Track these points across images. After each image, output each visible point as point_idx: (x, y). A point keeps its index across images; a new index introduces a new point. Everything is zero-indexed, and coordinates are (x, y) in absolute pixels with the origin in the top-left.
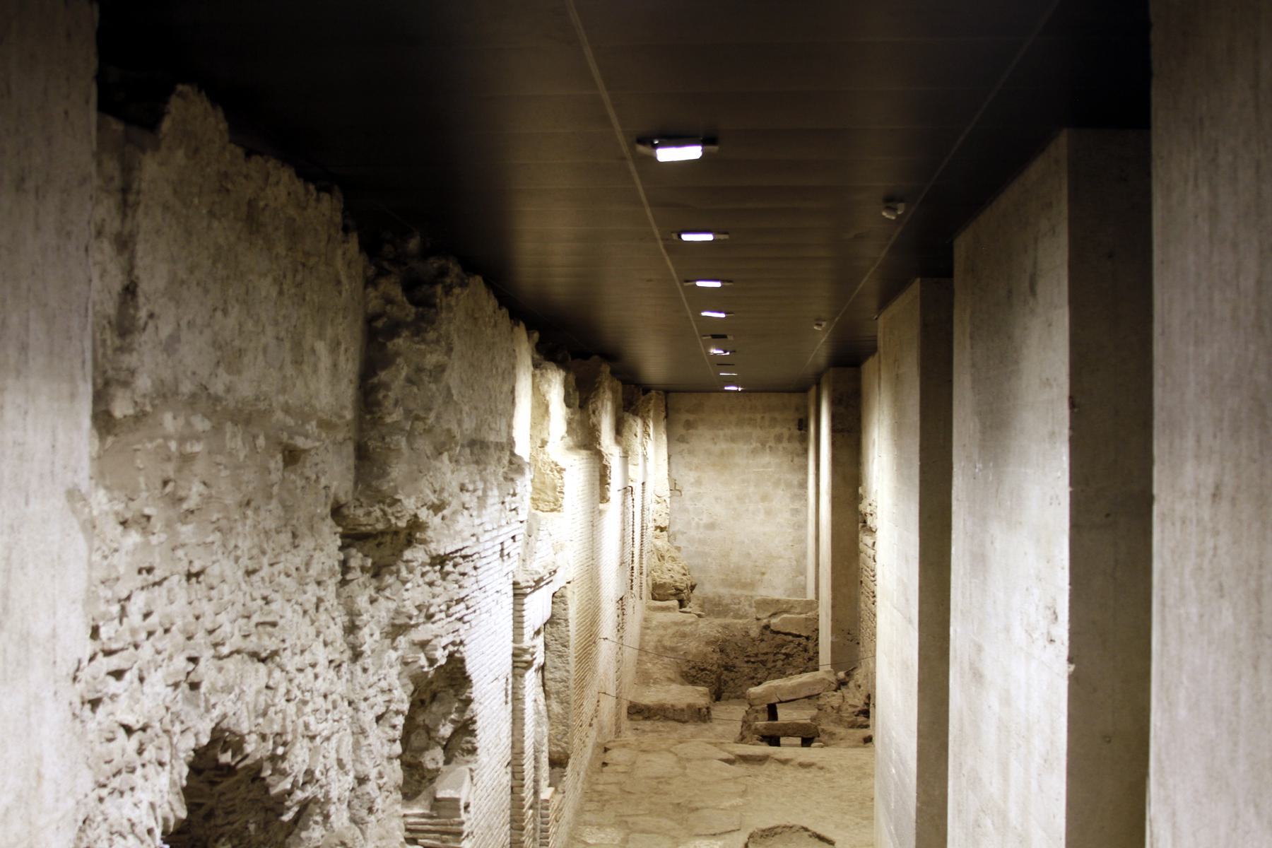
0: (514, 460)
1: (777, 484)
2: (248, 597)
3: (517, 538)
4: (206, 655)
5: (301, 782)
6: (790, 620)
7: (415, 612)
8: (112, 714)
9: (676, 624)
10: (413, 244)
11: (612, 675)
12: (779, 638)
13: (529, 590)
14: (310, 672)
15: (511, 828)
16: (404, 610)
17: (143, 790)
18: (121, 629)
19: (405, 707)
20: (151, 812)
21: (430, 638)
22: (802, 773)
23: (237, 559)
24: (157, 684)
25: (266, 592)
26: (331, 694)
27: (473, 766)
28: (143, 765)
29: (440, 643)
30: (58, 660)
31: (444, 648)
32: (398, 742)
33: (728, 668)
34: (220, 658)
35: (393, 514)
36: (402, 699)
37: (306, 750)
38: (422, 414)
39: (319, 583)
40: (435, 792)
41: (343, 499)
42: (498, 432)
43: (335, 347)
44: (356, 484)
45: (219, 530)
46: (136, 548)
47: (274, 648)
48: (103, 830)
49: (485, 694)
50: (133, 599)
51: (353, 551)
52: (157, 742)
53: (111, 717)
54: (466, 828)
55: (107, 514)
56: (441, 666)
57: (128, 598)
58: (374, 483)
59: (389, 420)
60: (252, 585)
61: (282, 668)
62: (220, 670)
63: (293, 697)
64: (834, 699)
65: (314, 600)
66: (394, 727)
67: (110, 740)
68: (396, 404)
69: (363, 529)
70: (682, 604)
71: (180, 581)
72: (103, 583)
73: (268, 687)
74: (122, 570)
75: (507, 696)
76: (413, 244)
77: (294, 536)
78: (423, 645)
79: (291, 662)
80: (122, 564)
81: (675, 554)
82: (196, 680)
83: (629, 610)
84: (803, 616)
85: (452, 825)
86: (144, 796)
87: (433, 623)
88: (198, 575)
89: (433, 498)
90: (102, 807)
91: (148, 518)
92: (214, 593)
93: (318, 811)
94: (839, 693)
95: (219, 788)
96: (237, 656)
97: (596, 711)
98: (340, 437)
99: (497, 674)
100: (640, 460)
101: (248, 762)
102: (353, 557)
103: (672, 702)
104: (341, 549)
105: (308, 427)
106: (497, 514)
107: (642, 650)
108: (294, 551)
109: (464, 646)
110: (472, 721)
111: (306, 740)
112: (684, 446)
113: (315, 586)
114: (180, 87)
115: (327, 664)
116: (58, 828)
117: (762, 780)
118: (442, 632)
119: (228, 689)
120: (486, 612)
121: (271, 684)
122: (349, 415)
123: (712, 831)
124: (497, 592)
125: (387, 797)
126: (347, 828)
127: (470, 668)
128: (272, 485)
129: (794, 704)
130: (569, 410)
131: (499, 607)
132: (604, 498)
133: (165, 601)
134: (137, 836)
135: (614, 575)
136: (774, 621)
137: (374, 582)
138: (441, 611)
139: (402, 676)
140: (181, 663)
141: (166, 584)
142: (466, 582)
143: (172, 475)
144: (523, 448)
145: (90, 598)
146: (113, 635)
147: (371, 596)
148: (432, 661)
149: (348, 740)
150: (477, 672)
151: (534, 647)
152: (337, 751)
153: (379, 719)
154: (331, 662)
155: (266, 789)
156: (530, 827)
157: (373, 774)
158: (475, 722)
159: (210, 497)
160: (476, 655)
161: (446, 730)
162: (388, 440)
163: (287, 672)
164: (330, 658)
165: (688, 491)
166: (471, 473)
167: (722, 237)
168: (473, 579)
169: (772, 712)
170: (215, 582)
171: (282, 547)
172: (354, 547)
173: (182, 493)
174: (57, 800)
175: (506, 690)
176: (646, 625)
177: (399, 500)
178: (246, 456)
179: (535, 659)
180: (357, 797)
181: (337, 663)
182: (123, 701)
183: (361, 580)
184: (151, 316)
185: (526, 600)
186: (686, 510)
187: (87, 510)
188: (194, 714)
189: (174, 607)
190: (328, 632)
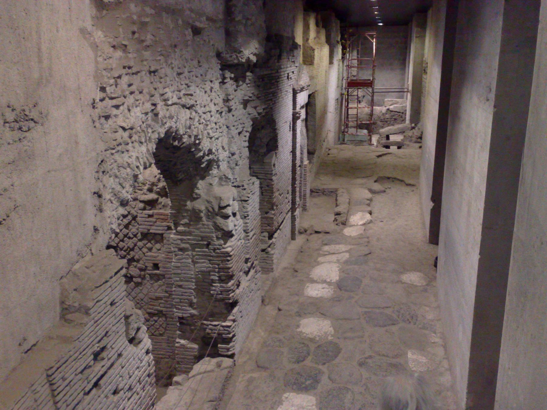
2: (179, 84)
3: (295, 72)
5: (207, 153)
12: (392, 113)
13: (298, 91)
18: (116, 89)
19: (250, 129)
20: (137, 160)
24: (137, 112)
25: (187, 82)
28: (132, 142)
30: (82, 98)
32: (247, 142)
34: (168, 106)
35: (240, 57)
37: (208, 142)
38: (250, 17)
39: (211, 81)
41: (221, 50)
44: (226, 45)
46: (120, 59)
53: (115, 123)
55: (104, 42)
58: (233, 44)
60: (180, 79)
62: (168, 110)
63: (201, 122)
64: (410, 133)
66: (245, 136)
67: (116, 132)
71: (146, 74)
72: (105, 70)
73: (190, 118)
75: (290, 128)
77: (199, 62)
80: (113, 63)
82: (157, 113)
86: (134, 155)
88: (154, 72)
91: (126, 46)
92: (162, 80)
93: (215, 164)
94: (412, 131)
95: (176, 155)
98: (218, 25)
101: (184, 145)
104: (220, 69)
105: (202, 19)
108: (199, 68)
109: (220, 83)
111: (209, 139)
113: (210, 83)
115: (216, 112)
116: (88, 163)
119: (171, 117)
121: (191, 117)
122: (221, 17)
128: (187, 41)
134: (131, 168)
135: (334, 90)
140: (148, 106)
141: (139, 74)
143: (136, 30)
144: (299, 40)
145: (97, 76)
146: (113, 91)
147: (234, 89)
152: (222, 143)
153: (240, 133)
154: (217, 111)
155: (194, 155)
157: (237, 152)
159: (156, 41)
162: (237, 27)
163: (199, 113)
164: (217, 109)
169: (388, 137)
170: (163, 76)
172: (227, 70)
173: (143, 38)
174: (87, 153)
175: (290, 126)
177: (242, 51)
178: (173, 27)
180: (231, 160)
181: (220, 111)
182: (121, 118)
187: (92, 38)
188: (156, 125)
189: (144, 84)
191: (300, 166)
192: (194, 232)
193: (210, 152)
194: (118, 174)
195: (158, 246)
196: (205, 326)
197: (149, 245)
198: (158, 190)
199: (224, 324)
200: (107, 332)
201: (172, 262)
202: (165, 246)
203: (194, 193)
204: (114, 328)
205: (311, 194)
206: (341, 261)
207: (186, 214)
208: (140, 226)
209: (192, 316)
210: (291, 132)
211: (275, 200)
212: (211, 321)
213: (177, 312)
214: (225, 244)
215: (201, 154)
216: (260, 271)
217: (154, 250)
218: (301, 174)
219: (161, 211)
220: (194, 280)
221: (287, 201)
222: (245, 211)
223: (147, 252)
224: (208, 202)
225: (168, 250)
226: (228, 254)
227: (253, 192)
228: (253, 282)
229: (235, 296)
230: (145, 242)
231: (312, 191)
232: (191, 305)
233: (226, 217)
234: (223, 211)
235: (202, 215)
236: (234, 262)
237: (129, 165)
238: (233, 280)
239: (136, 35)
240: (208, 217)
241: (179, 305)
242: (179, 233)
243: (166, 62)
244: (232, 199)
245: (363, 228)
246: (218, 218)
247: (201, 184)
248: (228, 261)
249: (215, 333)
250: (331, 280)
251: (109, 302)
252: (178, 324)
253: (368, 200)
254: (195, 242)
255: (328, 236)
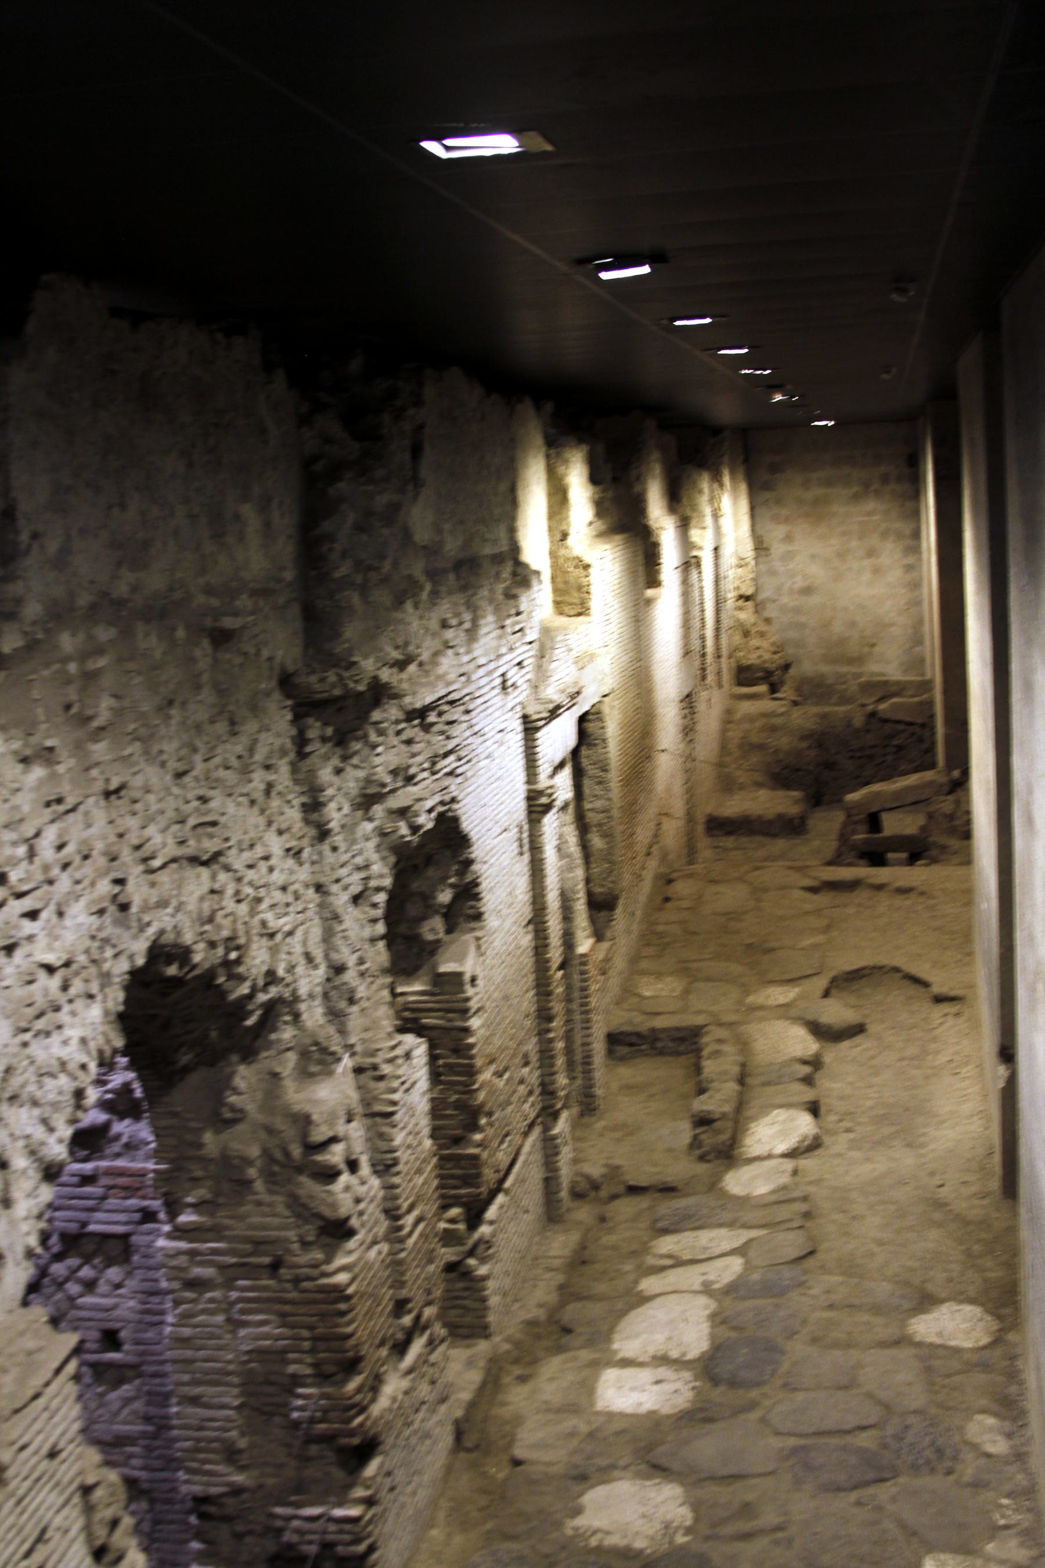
0: (519, 570)
1: (885, 535)
4: (135, 873)
6: (901, 704)
7: (388, 779)
8: (29, 955)
9: (765, 715)
10: (355, 365)
11: (678, 788)
12: (888, 728)
14: (263, 866)
15: (537, 994)
16: (375, 778)
17: (72, 1026)
18: (32, 867)
19: (388, 882)
21: (410, 803)
22: (899, 901)
23: (163, 764)
24: (79, 915)
26: (292, 884)
27: (479, 934)
29: (422, 806)
31: (430, 811)
33: (829, 766)
34: (152, 871)
36: (382, 874)
40: (435, 966)
41: (291, 668)
42: (495, 542)
43: (264, 505)
45: (138, 739)
46: (41, 782)
47: (216, 849)
48: (30, 1075)
49: (492, 849)
50: (44, 834)
51: (310, 721)
52: (84, 974)
54: (473, 1004)
56: (429, 831)
57: (37, 835)
59: (337, 574)
61: (227, 868)
65: (262, 787)
68: (344, 555)
69: (319, 696)
70: (774, 689)
71: (97, 802)
74: (26, 808)
75: (521, 846)
76: (355, 365)
77: (233, 723)
78: (403, 812)
79: (237, 860)
80: (25, 802)
81: (763, 627)
83: (701, 707)
84: (916, 699)
85: (458, 1002)
86: (74, 1033)
87: (415, 784)
88: (117, 791)
89: (396, 655)
90: (27, 1051)
91: (51, 749)
92: (138, 806)
94: (951, 798)
96: (174, 866)
97: (656, 836)
98: (281, 600)
99: (507, 824)
100: (709, 520)
101: (197, 972)
102: (310, 727)
103: (759, 812)
106: (494, 643)
107: (724, 748)
108: (233, 739)
109: (458, 802)
110: (475, 884)
112: (767, 495)
114: (45, 278)
117: (850, 910)
118: (425, 794)
119: (162, 904)
120: (487, 757)
122: (289, 575)
123: (787, 977)
124: (501, 731)
125: (372, 983)
126: (321, 1026)
127: (467, 825)
128: (199, 675)
129: (902, 809)
130: (597, 489)
131: (503, 748)
132: (653, 580)
133: (81, 826)
136: (882, 706)
137: (339, 751)
138: (424, 770)
139: (382, 847)
140: (105, 887)
141: (82, 808)
142: (455, 731)
143: (74, 697)
148: (415, 829)
149: (316, 932)
150: (477, 829)
151: (551, 787)
153: (356, 899)
154: (288, 850)
156: (560, 990)
157: (351, 960)
158: (477, 885)
160: (475, 809)
161: (445, 897)
163: (236, 871)
164: (288, 846)
165: (778, 549)
166: (456, 604)
167: (717, 319)
168: (465, 725)
169: (874, 822)
170: (137, 794)
171: (218, 738)
173: (89, 712)
175: (520, 840)
176: (728, 718)
177: (355, 663)
179: (554, 800)
180: (335, 988)
182: (42, 941)
183: (323, 751)
184: (35, 536)
185: (539, 735)
186: (773, 573)
188: (126, 935)
190: (282, 818)
191: (562, 966)
192: (228, 1228)
193: (271, 978)
194: (39, 1094)
195: (114, 1273)
196: (279, 1523)
197: (86, 1272)
198: (109, 1096)
199: (339, 1512)
200: (44, 1531)
201: (162, 1323)
202: (139, 1274)
203: (226, 1104)
204: (58, 1520)
205: (610, 1053)
206: (717, 1286)
207: (199, 1173)
208: (57, 1214)
209: (237, 1491)
210: (527, 857)
211: (481, 1096)
212: (299, 1505)
213: (186, 1482)
214: (328, 1260)
215: (245, 989)
216: (442, 1341)
217: (103, 1287)
218: (569, 988)
219: (121, 1163)
220: (236, 1380)
221: (522, 1089)
222: (385, 1148)
223: (81, 1296)
224: (270, 1131)
225: (148, 1285)
226: (338, 1293)
227: (406, 1086)
228: (423, 1376)
229: (369, 1423)
230: (73, 1262)
231: (613, 1039)
232: (231, 1455)
233: (330, 1175)
234: (319, 1158)
235: (252, 1172)
236: (360, 1318)
237: (63, 1064)
238: (360, 1373)
239: (74, 710)
240: (270, 1178)
241: (194, 1460)
242: (181, 1232)
243: (146, 752)
244: (342, 1120)
245: (789, 1165)
246: (303, 1179)
247: (243, 1078)
248: (343, 1314)
249: (310, 1542)
250: (684, 1354)
251: (45, 1451)
252: (193, 1519)
253: (805, 1062)
254: (234, 1260)
255: (668, 1207)
